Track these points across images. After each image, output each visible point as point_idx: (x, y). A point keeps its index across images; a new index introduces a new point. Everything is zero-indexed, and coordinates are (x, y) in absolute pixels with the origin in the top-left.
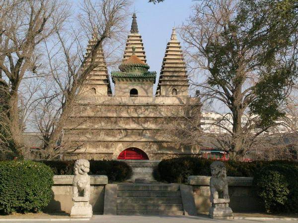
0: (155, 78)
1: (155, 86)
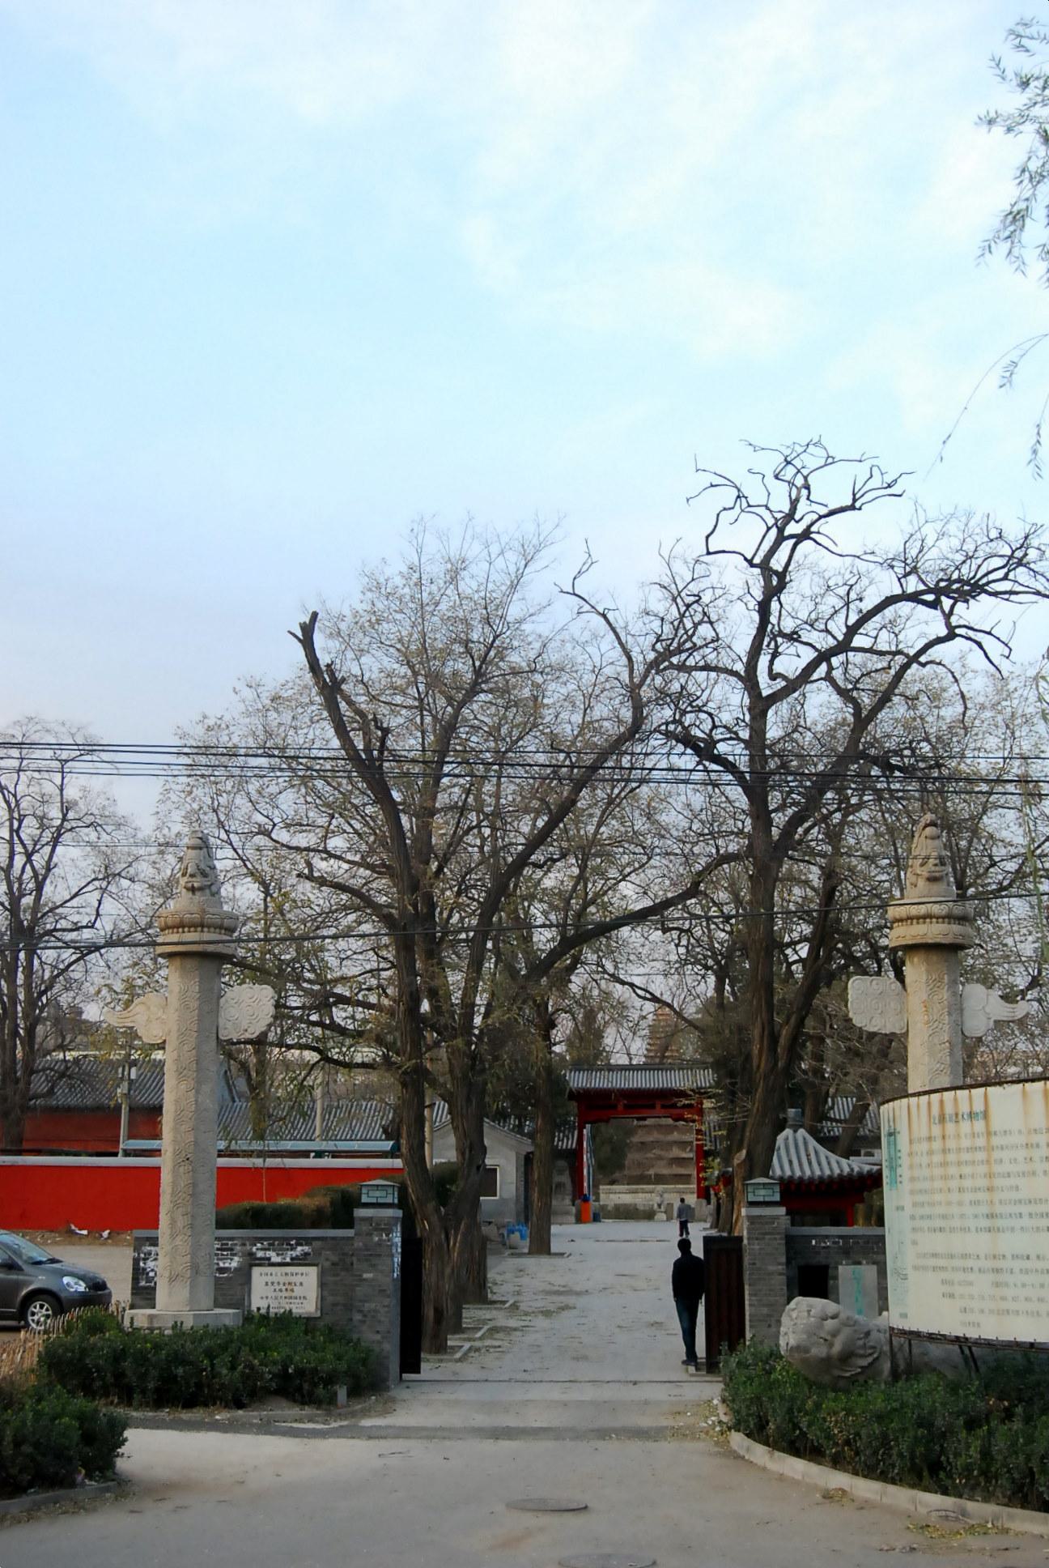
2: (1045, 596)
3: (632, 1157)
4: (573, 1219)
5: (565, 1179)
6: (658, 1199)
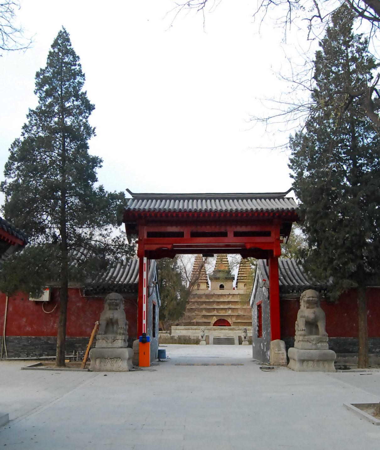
0: (233, 278)
1: (235, 282)
2: (1, 47)
3: (187, 314)
4: (124, 365)
5: (119, 315)
6: (202, 334)
